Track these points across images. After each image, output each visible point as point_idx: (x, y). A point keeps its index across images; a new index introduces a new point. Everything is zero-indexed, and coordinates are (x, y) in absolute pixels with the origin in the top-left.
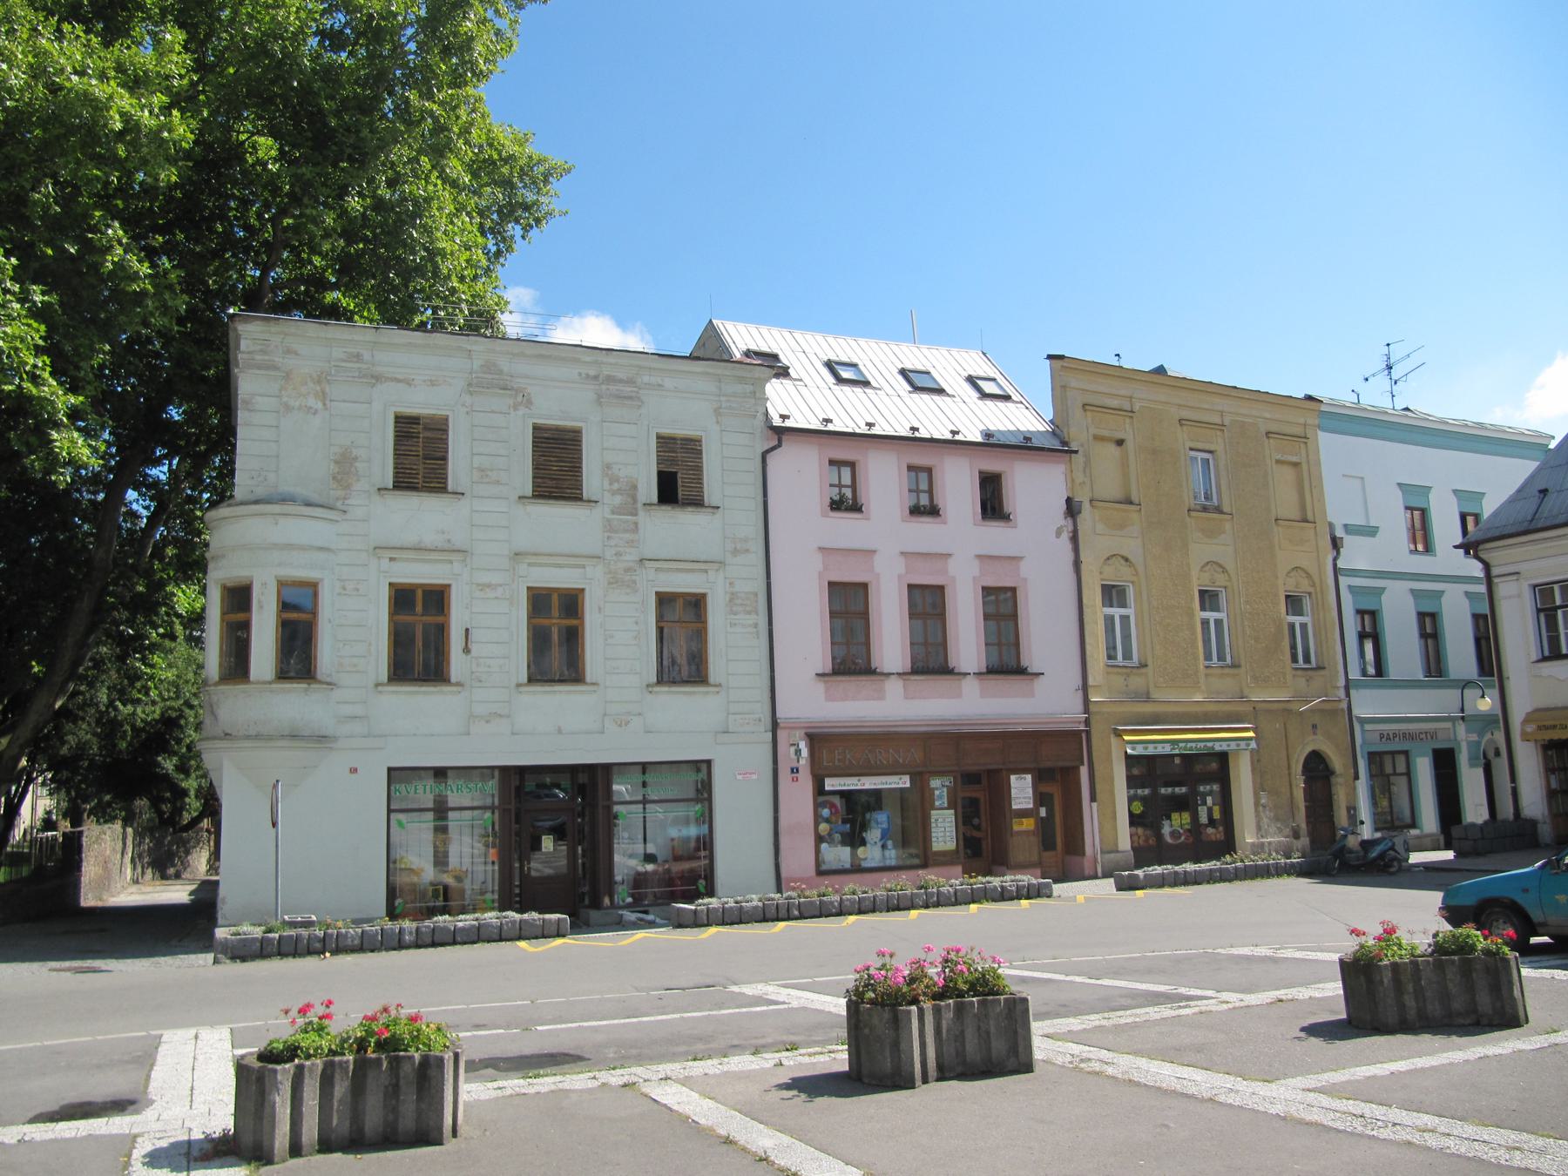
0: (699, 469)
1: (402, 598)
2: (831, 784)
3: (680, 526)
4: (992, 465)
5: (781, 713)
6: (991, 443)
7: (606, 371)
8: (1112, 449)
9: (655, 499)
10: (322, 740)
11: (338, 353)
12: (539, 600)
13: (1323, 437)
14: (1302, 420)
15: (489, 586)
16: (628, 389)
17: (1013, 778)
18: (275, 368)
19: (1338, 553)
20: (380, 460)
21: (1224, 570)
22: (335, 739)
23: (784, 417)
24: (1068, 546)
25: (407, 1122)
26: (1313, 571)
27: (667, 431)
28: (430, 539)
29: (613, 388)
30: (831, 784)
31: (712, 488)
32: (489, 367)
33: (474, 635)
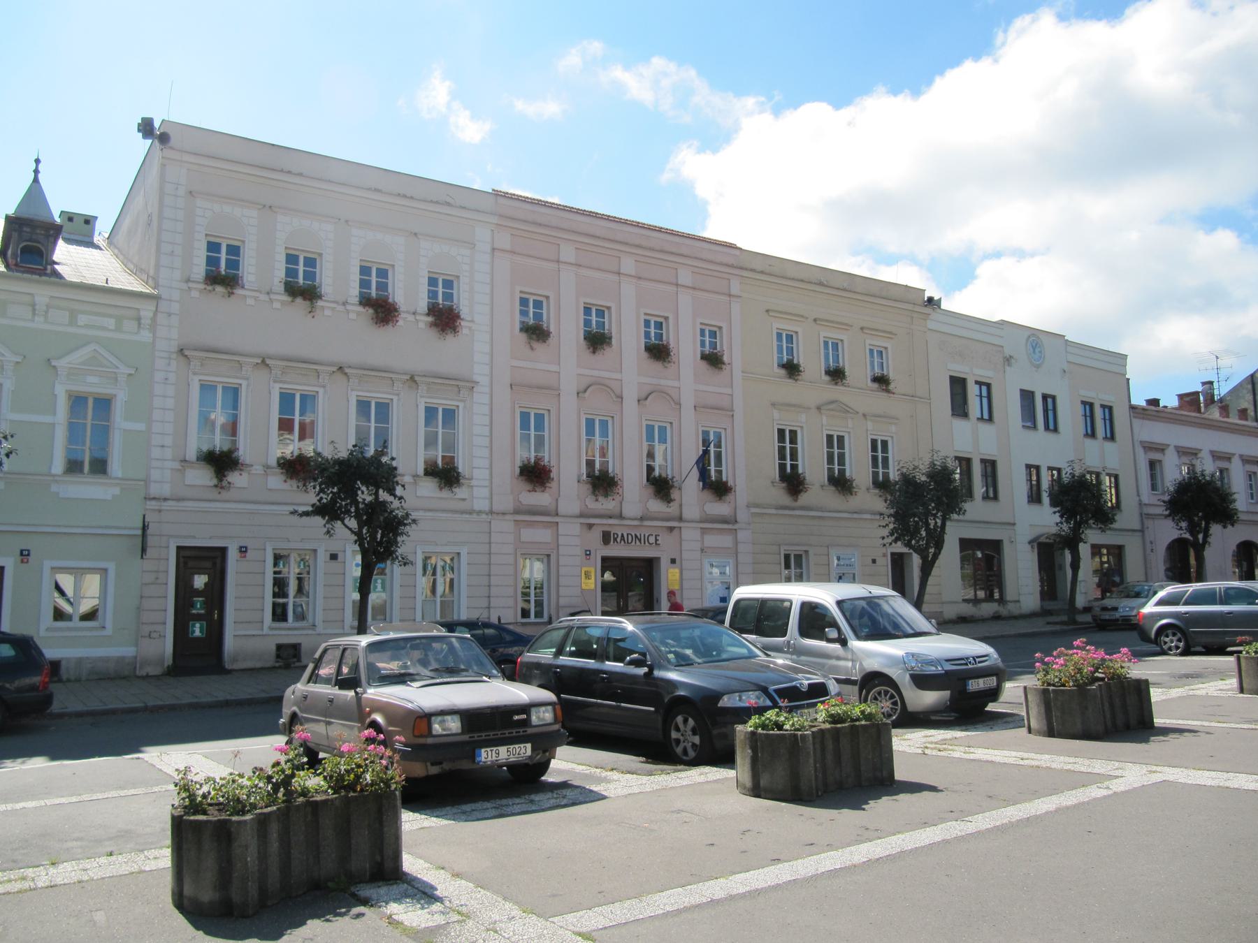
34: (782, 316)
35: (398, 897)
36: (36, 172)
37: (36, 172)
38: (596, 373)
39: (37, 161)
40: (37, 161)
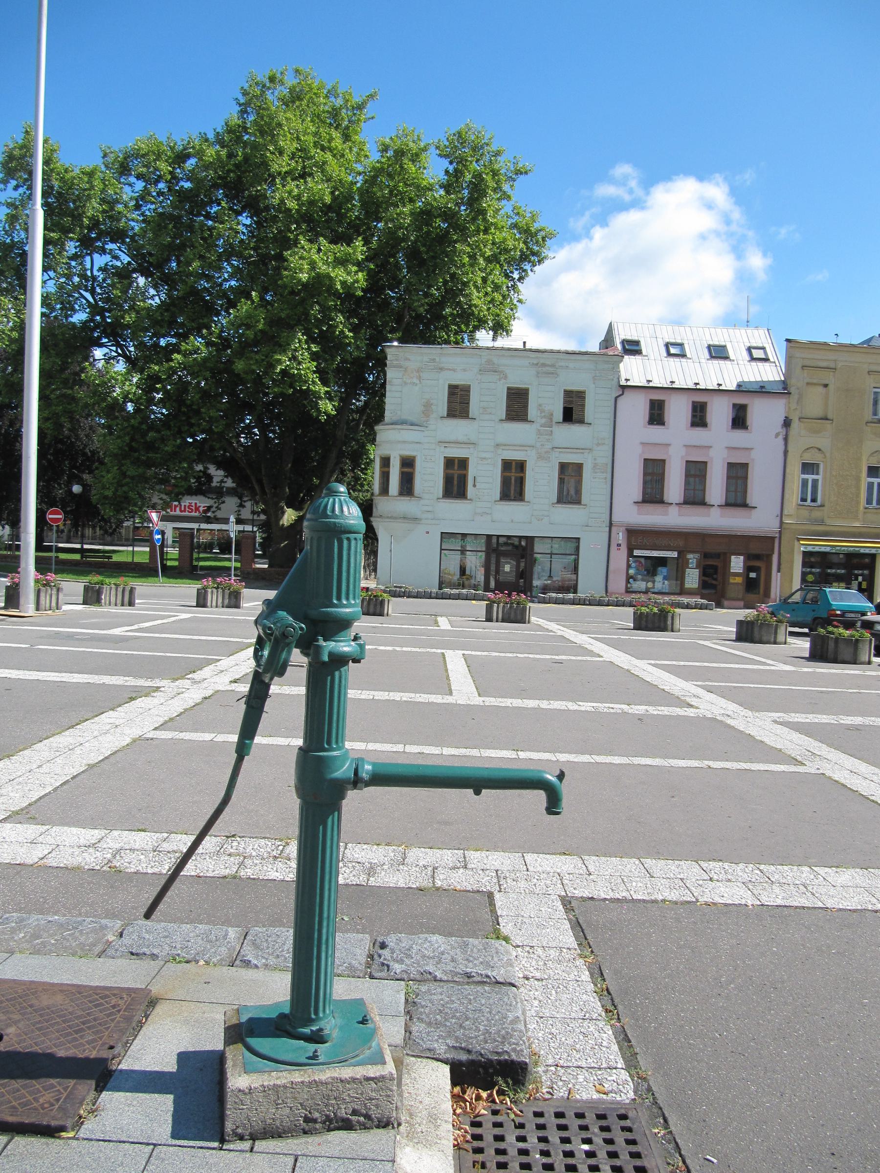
0: (583, 406)
1: (449, 462)
2: (636, 553)
3: (574, 431)
4: (741, 400)
5: (614, 519)
6: (742, 389)
7: (542, 361)
8: (821, 389)
10: (415, 520)
11: (426, 359)
12: (507, 465)
15: (485, 458)
16: (551, 369)
17: (733, 557)
18: (401, 367)
20: (442, 405)
22: (421, 519)
23: (627, 380)
24: (782, 443)
27: (569, 388)
28: (461, 438)
29: (545, 369)
30: (636, 553)
32: (489, 362)
33: (478, 479)
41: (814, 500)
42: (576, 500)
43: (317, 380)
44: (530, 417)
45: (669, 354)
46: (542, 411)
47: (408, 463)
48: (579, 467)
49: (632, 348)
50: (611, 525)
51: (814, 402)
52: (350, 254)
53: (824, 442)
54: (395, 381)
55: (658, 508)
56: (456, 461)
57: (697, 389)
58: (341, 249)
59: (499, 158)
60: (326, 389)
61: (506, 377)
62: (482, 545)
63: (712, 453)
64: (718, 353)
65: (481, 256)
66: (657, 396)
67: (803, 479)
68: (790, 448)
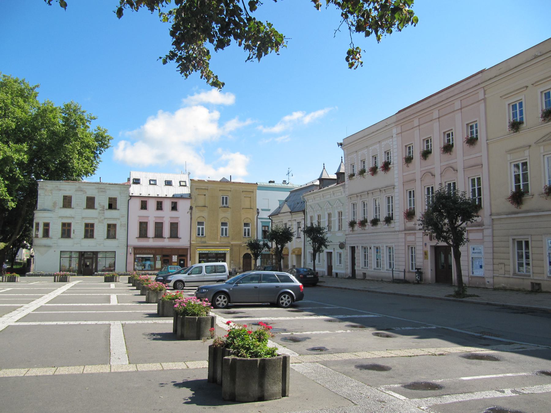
0: (116, 203)
1: (64, 225)
2: (138, 256)
3: (113, 213)
4: (174, 200)
5: (128, 244)
6: (174, 197)
7: (100, 187)
8: (203, 196)
9: (108, 208)
10: (49, 246)
11: (54, 186)
12: (87, 225)
13: (258, 192)
14: (253, 188)
15: (78, 223)
16: (103, 190)
17: (173, 256)
18: (44, 189)
19: (258, 215)
20: (61, 203)
21: (228, 219)
22: (52, 246)
23: (132, 194)
24: (190, 215)
25: (14, 280)
26: (252, 219)
27: (111, 197)
28: (68, 215)
29: (101, 190)
30: (138, 256)
31: (118, 206)
32: (79, 187)
33: (75, 231)
34: (509, 95)
35: (472, 387)
36: (324, 166)
37: (324, 166)
38: (426, 168)
39: (324, 164)
40: (324, 164)
41: (202, 235)
42: (114, 237)
43: (7, 194)
44: (96, 207)
45: (150, 184)
46: (100, 205)
47: (47, 225)
48: (115, 226)
49: (137, 182)
50: (468, 251)
51: (201, 201)
52: (22, 148)
53: (205, 214)
54: (42, 194)
55: (176, 240)
56: (90, 225)
57: (166, 197)
58: (18, 146)
59: (84, 114)
60: (11, 198)
61: (86, 193)
62: (77, 255)
63: (165, 219)
64: (169, 183)
65: (76, 149)
66: (160, 200)
67: (198, 228)
68: (193, 216)
